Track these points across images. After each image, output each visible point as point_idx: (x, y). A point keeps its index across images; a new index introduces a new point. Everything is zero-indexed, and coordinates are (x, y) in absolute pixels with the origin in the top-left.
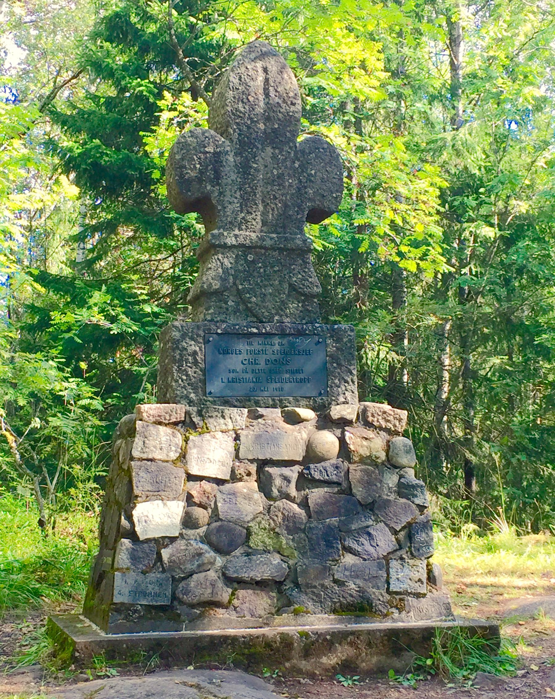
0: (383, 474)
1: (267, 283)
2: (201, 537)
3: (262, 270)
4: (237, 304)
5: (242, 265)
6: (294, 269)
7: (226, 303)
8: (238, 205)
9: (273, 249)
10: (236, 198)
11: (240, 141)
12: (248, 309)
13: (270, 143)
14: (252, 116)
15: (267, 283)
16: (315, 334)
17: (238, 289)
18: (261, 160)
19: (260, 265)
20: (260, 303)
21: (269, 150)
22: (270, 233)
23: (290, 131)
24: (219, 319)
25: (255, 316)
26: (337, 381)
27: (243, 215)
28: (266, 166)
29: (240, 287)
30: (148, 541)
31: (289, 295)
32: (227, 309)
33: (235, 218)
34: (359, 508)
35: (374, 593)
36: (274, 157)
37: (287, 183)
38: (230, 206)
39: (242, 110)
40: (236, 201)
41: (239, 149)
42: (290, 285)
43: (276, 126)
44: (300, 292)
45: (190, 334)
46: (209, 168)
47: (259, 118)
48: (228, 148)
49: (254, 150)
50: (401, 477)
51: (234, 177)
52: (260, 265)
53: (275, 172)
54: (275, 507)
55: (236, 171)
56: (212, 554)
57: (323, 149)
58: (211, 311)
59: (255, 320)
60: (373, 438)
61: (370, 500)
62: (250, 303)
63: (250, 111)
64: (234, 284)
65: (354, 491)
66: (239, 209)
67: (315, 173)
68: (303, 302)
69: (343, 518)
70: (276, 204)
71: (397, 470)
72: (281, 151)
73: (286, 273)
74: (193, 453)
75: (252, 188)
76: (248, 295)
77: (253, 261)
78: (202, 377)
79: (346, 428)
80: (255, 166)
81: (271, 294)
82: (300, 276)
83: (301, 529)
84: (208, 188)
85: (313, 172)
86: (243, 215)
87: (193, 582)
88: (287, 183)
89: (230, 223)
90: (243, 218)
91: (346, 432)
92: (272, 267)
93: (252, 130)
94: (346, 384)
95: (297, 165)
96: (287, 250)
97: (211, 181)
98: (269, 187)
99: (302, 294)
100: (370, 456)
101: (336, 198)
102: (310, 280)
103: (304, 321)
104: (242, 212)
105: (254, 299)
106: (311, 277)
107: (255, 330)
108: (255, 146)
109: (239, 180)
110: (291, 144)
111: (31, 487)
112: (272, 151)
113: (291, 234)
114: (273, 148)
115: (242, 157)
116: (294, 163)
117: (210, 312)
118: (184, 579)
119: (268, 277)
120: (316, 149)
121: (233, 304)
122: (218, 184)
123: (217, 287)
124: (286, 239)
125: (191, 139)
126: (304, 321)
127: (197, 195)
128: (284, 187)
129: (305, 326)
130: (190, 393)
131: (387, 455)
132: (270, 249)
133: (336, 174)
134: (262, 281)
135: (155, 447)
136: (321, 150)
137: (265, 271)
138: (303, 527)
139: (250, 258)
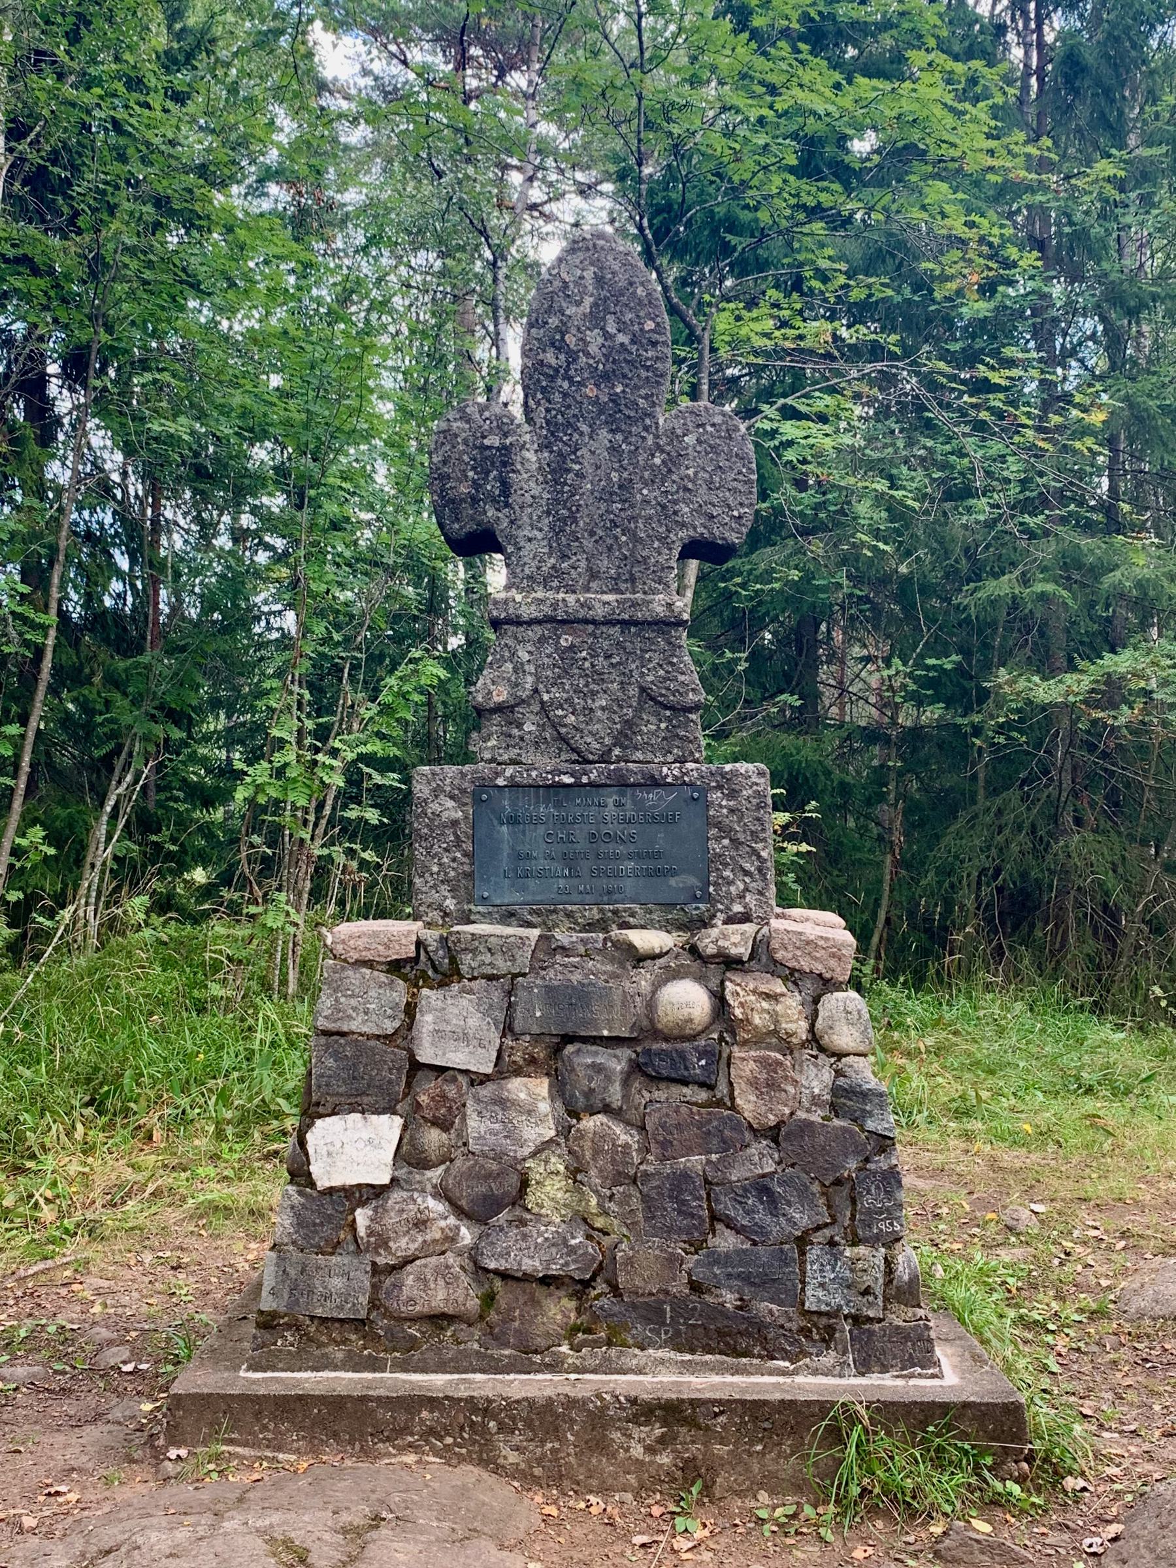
0: (801, 1065)
1: (596, 688)
2: (435, 1187)
3: (587, 664)
4: (542, 727)
5: (549, 656)
6: (650, 660)
7: (520, 726)
8: (545, 543)
9: (609, 622)
10: (541, 530)
11: (548, 422)
12: (562, 739)
13: (607, 423)
14: (572, 372)
15: (596, 688)
16: (684, 783)
17: (542, 702)
18: (588, 455)
19: (584, 654)
20: (583, 726)
21: (604, 434)
22: (603, 592)
23: (646, 397)
24: (506, 757)
25: (573, 750)
26: (727, 873)
27: (553, 561)
28: (598, 467)
29: (546, 697)
30: (331, 1191)
31: (639, 709)
32: (522, 739)
33: (539, 568)
34: (748, 1136)
35: (771, 1312)
36: (614, 449)
37: (639, 497)
38: (528, 546)
39: (553, 362)
40: (539, 535)
41: (546, 437)
42: (643, 690)
43: (619, 390)
44: (661, 703)
45: (448, 789)
46: (492, 475)
47: (586, 375)
48: (527, 437)
49: (576, 436)
50: (839, 1073)
51: (536, 490)
52: (584, 654)
53: (615, 476)
54: (578, 1130)
55: (541, 479)
56: (452, 1220)
57: (713, 425)
58: (492, 742)
59: (575, 757)
60: (783, 995)
61: (772, 1120)
62: (565, 726)
63: (569, 364)
64: (536, 691)
65: (738, 1101)
66: (546, 550)
67: (696, 474)
68: (669, 720)
69: (714, 1157)
70: (616, 538)
71: (833, 1060)
72: (627, 436)
73: (633, 666)
74: (426, 1021)
75: (570, 509)
76: (560, 712)
77: (572, 647)
78: (467, 868)
79: (728, 974)
80: (577, 467)
81: (603, 709)
82: (661, 672)
83: (627, 1176)
84: (489, 514)
85: (691, 472)
86: (553, 561)
87: (409, 1279)
88: (639, 497)
89: (530, 577)
90: (553, 567)
91: (728, 983)
92: (608, 657)
93: (569, 401)
94: (747, 880)
95: (657, 461)
96: (636, 623)
97: (494, 501)
98: (603, 506)
99: (666, 707)
100: (775, 1032)
101: (740, 517)
102: (681, 678)
103: (670, 758)
104: (550, 555)
105: (572, 719)
106: (683, 673)
107: (567, 780)
108: (576, 429)
109: (546, 496)
110: (648, 421)
111: (398, 934)
112: (610, 436)
113: (645, 593)
114: (611, 431)
115: (551, 452)
116: (653, 456)
117: (489, 744)
118: (394, 1268)
119: (599, 676)
120: (699, 426)
121: (533, 728)
122: (507, 505)
123: (501, 699)
124: (634, 604)
125: (459, 424)
126: (670, 758)
127: (471, 527)
128: (632, 506)
129: (665, 770)
130: (446, 898)
131: (812, 1029)
132: (603, 623)
133: (740, 473)
134: (587, 685)
135: (354, 1009)
136: (709, 428)
137: (593, 666)
138: (632, 1172)
139: (566, 641)
